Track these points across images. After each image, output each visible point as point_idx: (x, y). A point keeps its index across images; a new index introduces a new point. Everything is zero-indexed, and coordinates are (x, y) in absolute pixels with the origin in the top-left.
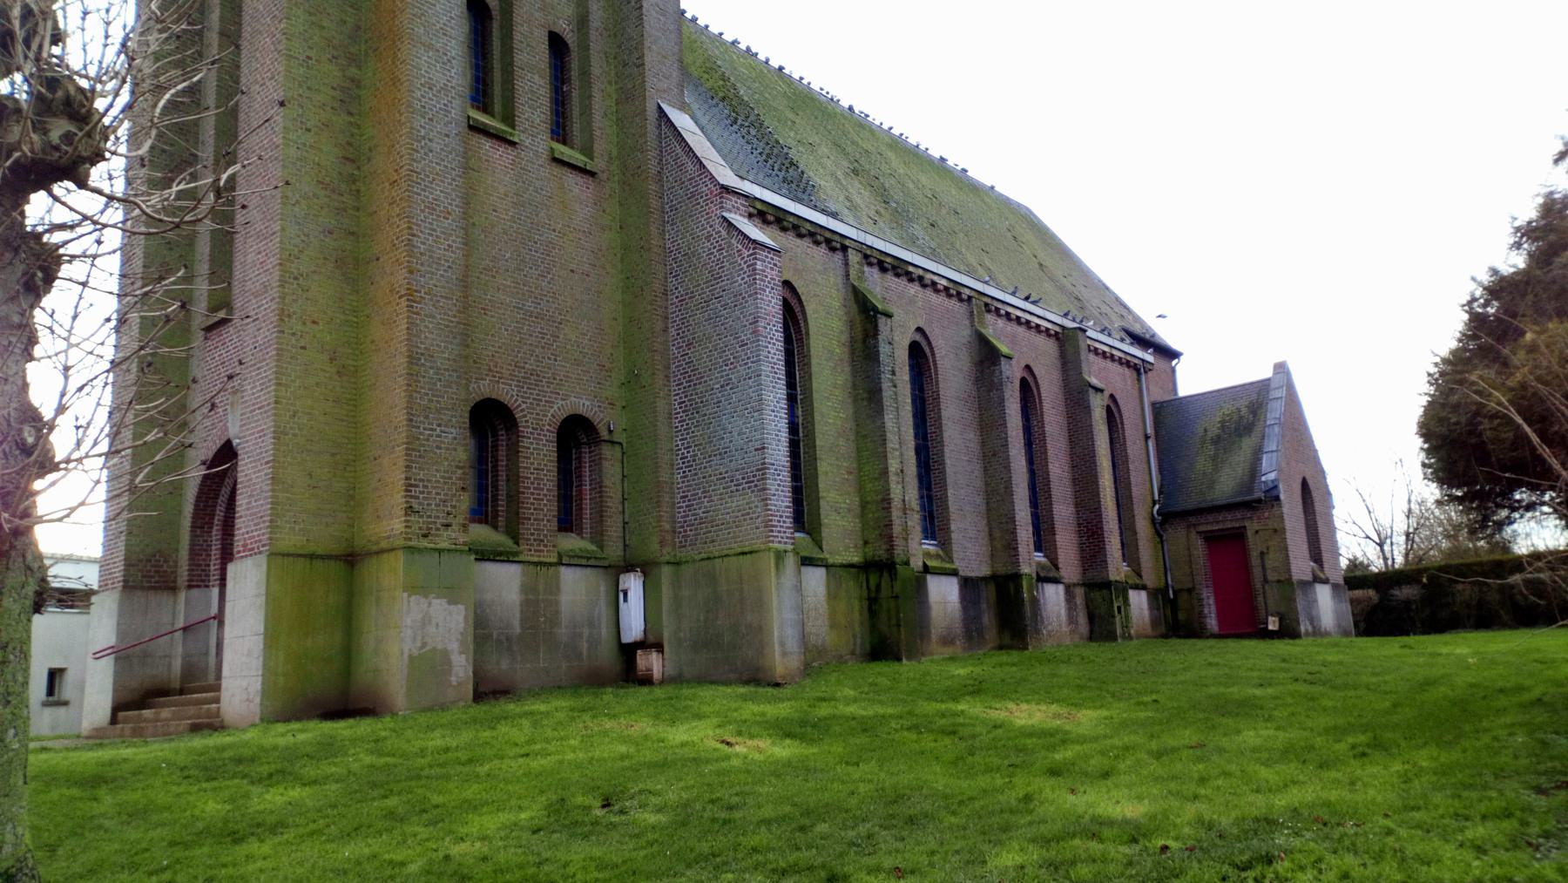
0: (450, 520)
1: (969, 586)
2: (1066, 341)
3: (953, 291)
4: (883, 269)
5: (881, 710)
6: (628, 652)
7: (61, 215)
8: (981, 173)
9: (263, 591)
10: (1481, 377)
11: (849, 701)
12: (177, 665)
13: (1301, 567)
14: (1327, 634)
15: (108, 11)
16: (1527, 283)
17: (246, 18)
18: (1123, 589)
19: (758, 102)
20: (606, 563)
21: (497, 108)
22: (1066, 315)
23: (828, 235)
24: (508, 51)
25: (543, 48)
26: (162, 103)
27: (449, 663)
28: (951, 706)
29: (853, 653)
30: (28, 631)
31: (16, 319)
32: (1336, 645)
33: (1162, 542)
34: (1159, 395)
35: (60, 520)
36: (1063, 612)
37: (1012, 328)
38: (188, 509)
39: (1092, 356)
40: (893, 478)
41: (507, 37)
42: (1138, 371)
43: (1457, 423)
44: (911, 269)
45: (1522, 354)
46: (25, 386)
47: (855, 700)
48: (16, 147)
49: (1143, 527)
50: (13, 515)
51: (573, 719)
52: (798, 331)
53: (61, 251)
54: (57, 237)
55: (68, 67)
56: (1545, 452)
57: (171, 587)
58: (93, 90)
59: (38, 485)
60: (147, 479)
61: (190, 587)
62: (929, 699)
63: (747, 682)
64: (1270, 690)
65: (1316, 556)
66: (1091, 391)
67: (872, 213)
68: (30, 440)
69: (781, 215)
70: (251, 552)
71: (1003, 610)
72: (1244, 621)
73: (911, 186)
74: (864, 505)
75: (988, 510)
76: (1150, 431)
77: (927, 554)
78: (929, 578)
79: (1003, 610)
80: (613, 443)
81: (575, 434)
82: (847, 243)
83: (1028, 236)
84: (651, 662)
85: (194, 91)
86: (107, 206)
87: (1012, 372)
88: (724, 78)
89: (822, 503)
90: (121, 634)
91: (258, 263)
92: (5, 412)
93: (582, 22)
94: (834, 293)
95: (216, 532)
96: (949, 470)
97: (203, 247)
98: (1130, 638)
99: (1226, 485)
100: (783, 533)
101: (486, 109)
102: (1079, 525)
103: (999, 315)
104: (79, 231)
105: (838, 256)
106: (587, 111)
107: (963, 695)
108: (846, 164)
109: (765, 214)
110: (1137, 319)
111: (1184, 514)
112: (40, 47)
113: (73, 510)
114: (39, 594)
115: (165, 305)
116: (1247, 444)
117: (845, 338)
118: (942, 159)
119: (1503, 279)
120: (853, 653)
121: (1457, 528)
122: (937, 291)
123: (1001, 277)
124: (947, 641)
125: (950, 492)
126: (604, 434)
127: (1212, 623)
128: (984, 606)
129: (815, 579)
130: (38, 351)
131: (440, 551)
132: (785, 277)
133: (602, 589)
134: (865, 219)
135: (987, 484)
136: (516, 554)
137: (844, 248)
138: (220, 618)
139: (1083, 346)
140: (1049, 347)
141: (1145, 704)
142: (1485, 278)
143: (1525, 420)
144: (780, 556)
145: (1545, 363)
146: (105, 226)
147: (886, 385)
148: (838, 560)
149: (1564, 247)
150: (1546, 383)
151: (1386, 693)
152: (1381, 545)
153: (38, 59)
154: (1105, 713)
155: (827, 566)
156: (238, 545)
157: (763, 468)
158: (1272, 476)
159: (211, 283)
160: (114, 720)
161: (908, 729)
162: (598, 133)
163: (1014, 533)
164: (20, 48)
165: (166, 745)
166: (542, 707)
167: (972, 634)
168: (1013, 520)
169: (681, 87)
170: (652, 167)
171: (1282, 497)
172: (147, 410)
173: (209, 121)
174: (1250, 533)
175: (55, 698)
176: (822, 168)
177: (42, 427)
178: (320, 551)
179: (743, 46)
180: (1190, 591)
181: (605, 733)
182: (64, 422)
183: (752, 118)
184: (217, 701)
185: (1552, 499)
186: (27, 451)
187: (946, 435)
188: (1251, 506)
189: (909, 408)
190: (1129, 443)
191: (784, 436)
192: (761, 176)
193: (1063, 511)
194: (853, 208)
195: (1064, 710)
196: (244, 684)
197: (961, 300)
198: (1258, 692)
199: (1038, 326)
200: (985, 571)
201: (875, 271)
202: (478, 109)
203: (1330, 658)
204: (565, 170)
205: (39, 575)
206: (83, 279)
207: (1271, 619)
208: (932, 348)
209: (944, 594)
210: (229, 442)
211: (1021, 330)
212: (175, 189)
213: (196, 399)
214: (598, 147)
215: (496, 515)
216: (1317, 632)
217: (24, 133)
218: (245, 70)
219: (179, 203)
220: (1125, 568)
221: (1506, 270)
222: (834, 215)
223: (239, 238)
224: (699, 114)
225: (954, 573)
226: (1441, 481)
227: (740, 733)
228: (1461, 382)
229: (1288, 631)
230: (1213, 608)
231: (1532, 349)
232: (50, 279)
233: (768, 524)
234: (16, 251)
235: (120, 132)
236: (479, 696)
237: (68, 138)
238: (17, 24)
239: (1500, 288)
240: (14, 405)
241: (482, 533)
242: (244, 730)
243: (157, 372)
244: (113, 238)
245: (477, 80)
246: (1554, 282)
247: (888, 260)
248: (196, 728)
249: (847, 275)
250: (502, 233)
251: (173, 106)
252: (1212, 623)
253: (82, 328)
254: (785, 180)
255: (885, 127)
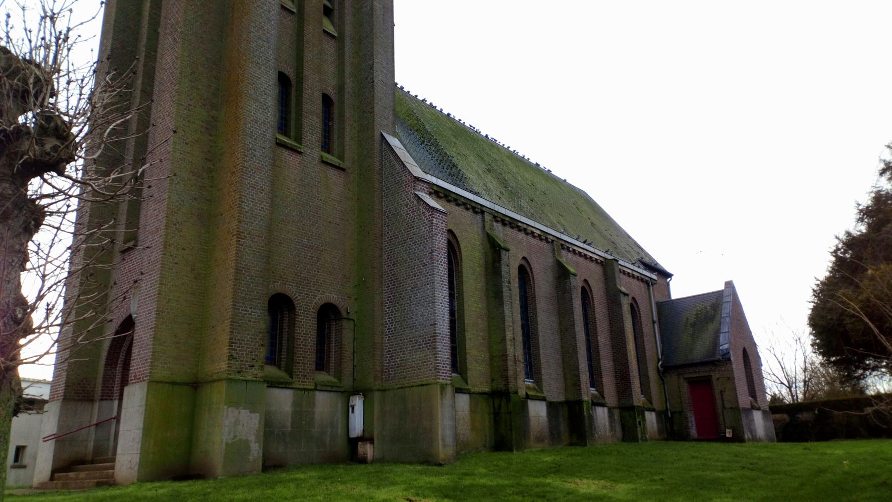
0: (254, 363)
1: (552, 407)
2: (607, 266)
3: (543, 237)
4: (504, 224)
5: (501, 482)
6: (353, 443)
7: (47, 190)
8: (558, 172)
9: (144, 403)
10: (844, 294)
11: (482, 476)
12: (91, 445)
13: (744, 400)
14: (760, 440)
15: (82, 80)
16: (868, 241)
17: (156, 83)
18: (641, 411)
19: (436, 132)
20: (342, 390)
21: (292, 133)
22: (607, 252)
23: (474, 205)
24: (299, 103)
25: (319, 102)
26: (108, 130)
27: (248, 448)
28: (542, 480)
29: (484, 446)
30: (9, 427)
31: (17, 247)
32: (766, 447)
33: (663, 383)
34: (661, 299)
35: (33, 362)
36: (607, 423)
37: (576, 258)
38: (104, 354)
39: (622, 275)
40: (508, 343)
41: (300, 96)
42: (648, 284)
43: (831, 319)
44: (520, 224)
45: (866, 282)
46: (19, 286)
47: (486, 475)
48: (27, 153)
49: (653, 375)
50: (6, 359)
51: (319, 483)
52: (456, 258)
53: (46, 209)
54: (44, 202)
55: (58, 110)
56: (883, 339)
57: (91, 400)
58: (71, 122)
59: (22, 341)
60: (84, 339)
61: (102, 400)
62: (529, 475)
63: (422, 463)
64: (729, 474)
65: (753, 393)
66: (622, 295)
67: (498, 193)
68: (20, 316)
69: (447, 193)
70: (138, 380)
71: (572, 422)
72: (712, 432)
73: (520, 179)
74: (492, 358)
75: (563, 362)
76: (655, 318)
77: (528, 388)
78: (529, 401)
79: (572, 422)
80: (349, 319)
81: (328, 314)
82: (484, 209)
83: (585, 207)
84: (367, 450)
85: (125, 124)
86: (73, 185)
87: (577, 283)
88: (418, 120)
89: (468, 356)
90: (60, 427)
91: (154, 217)
92: (7, 300)
93: (341, 88)
94: (476, 237)
95: (119, 368)
96: (541, 339)
97: (124, 207)
98: (646, 440)
99: (699, 351)
100: (445, 374)
101: (286, 134)
102: (616, 372)
103: (569, 251)
104: (58, 198)
105: (479, 217)
106: (342, 136)
107: (549, 473)
108: (484, 166)
109: (438, 193)
110: (647, 255)
111: (677, 367)
112: (44, 99)
113: (41, 356)
114: (17, 405)
115: (100, 240)
116: (711, 327)
117: (482, 262)
118: (537, 165)
119: (854, 238)
120: (484, 446)
121: (834, 379)
122: (534, 237)
123: (570, 230)
124: (540, 439)
125: (541, 351)
126: (344, 314)
127: (694, 432)
128: (561, 419)
129: (463, 401)
130: (28, 265)
131: (247, 381)
132: (450, 227)
133: (340, 405)
134: (494, 196)
135: (562, 347)
136: (291, 383)
137: (483, 212)
138: (118, 419)
139: (616, 269)
140: (598, 269)
141: (655, 481)
142: (843, 236)
143: (870, 319)
144: (443, 387)
145: (880, 288)
146: (71, 196)
147: (505, 289)
148: (477, 390)
149: (888, 221)
150: (881, 300)
151: (796, 477)
152: (790, 387)
153: (42, 106)
154: (631, 486)
155: (470, 393)
156: (131, 376)
157: (434, 336)
158: (726, 346)
159: (126, 229)
160: (52, 478)
161: (517, 494)
162: (347, 148)
163: (578, 376)
164: (32, 99)
165: (81, 495)
166: (302, 476)
167: (554, 436)
168: (577, 369)
169: (394, 124)
170: (377, 166)
171: (732, 359)
172: (88, 299)
173: (131, 140)
174: (714, 379)
175: (19, 463)
176: (471, 168)
177: (27, 308)
178: (178, 381)
179: (428, 103)
180: (680, 413)
181: (338, 493)
182: (42, 305)
183: (432, 141)
184: (113, 468)
185: (887, 364)
186: (17, 322)
187: (539, 318)
188: (714, 363)
189: (518, 302)
190: (644, 325)
191: (447, 317)
192: (437, 172)
193: (606, 364)
194: (488, 190)
195: (608, 484)
196: (129, 458)
197: (548, 242)
198: (721, 475)
199: (591, 257)
200: (562, 398)
201: (500, 225)
202: (282, 134)
203: (763, 455)
204: (329, 167)
205: (18, 394)
206: (57, 225)
207: (727, 430)
208: (531, 269)
209: (538, 411)
210: (130, 316)
211: (581, 260)
212: (112, 177)
213: (114, 293)
214: (347, 155)
215: (280, 360)
216: (755, 439)
217: (31, 145)
218: (154, 111)
219: (114, 184)
220: (642, 398)
221: (855, 233)
222: (477, 194)
223: (144, 205)
224: (403, 138)
225: (543, 399)
226: (823, 354)
227: (418, 495)
228: (832, 296)
229: (738, 438)
230: (694, 423)
231: (872, 278)
232: (37, 227)
233: (436, 368)
234: (21, 209)
235: (84, 145)
236: (265, 468)
237: (55, 148)
238: (31, 86)
239: (851, 242)
240: (13, 296)
241: (272, 371)
242: (127, 487)
243: (91, 275)
244: (74, 202)
245: (282, 118)
246: (883, 241)
247: (507, 219)
248: (99, 485)
249: (484, 227)
250: (290, 198)
251: (114, 132)
252: (694, 432)
253: (54, 253)
254: (450, 174)
255: (506, 146)
